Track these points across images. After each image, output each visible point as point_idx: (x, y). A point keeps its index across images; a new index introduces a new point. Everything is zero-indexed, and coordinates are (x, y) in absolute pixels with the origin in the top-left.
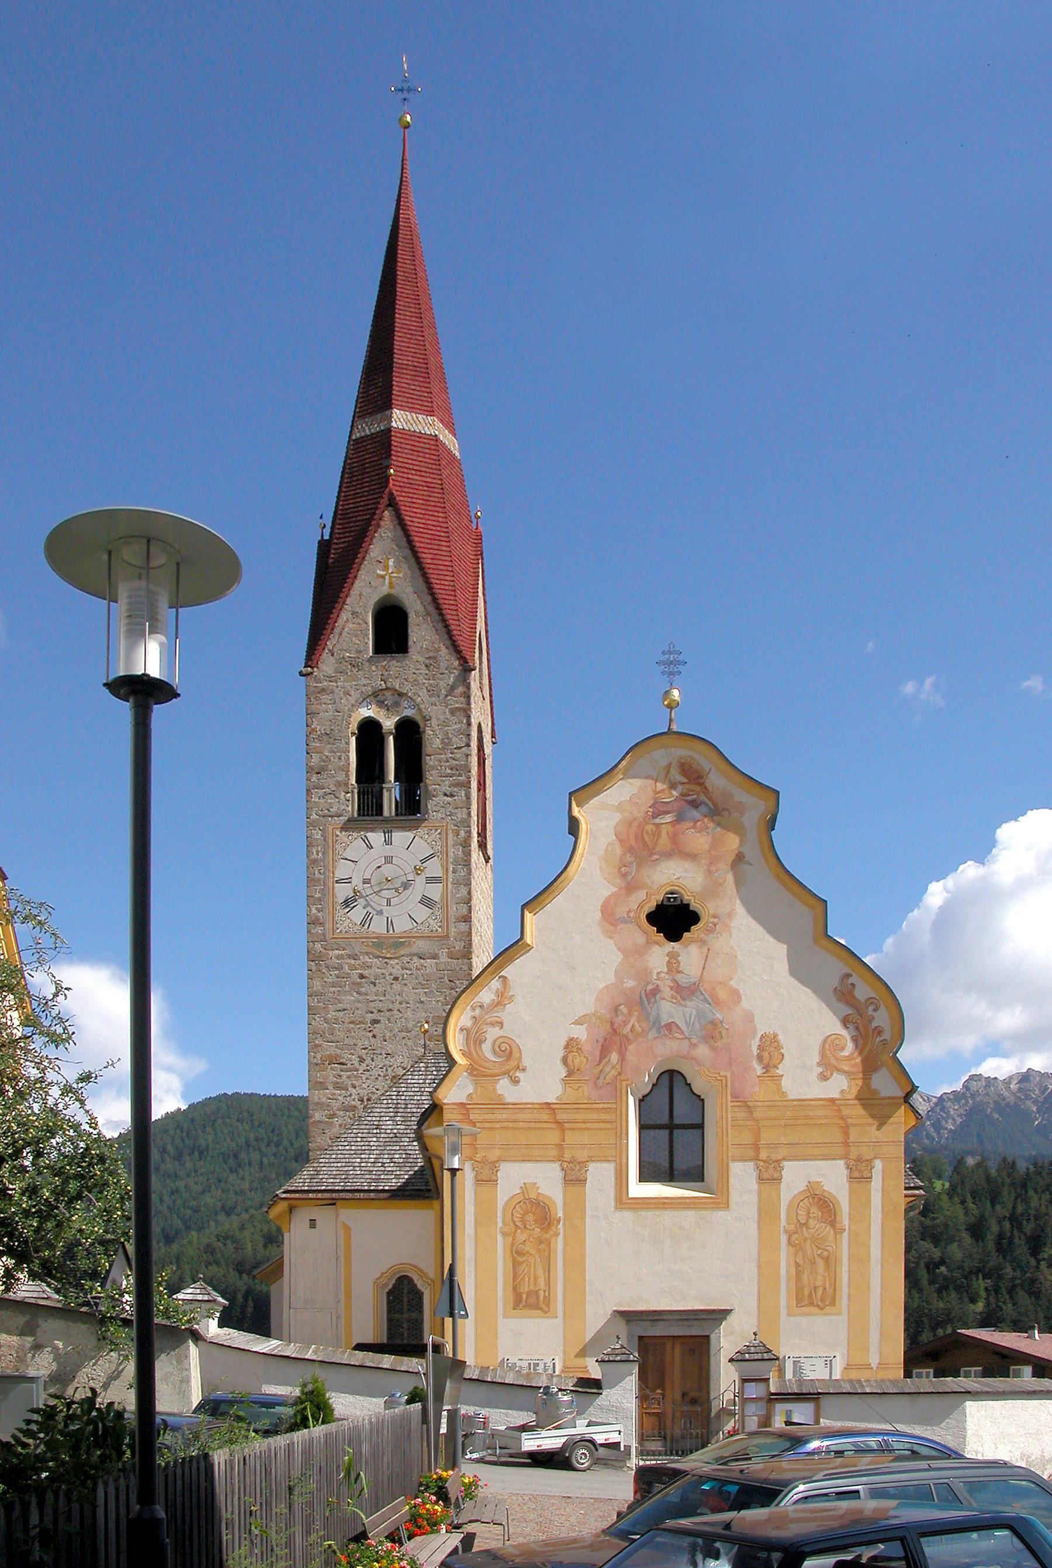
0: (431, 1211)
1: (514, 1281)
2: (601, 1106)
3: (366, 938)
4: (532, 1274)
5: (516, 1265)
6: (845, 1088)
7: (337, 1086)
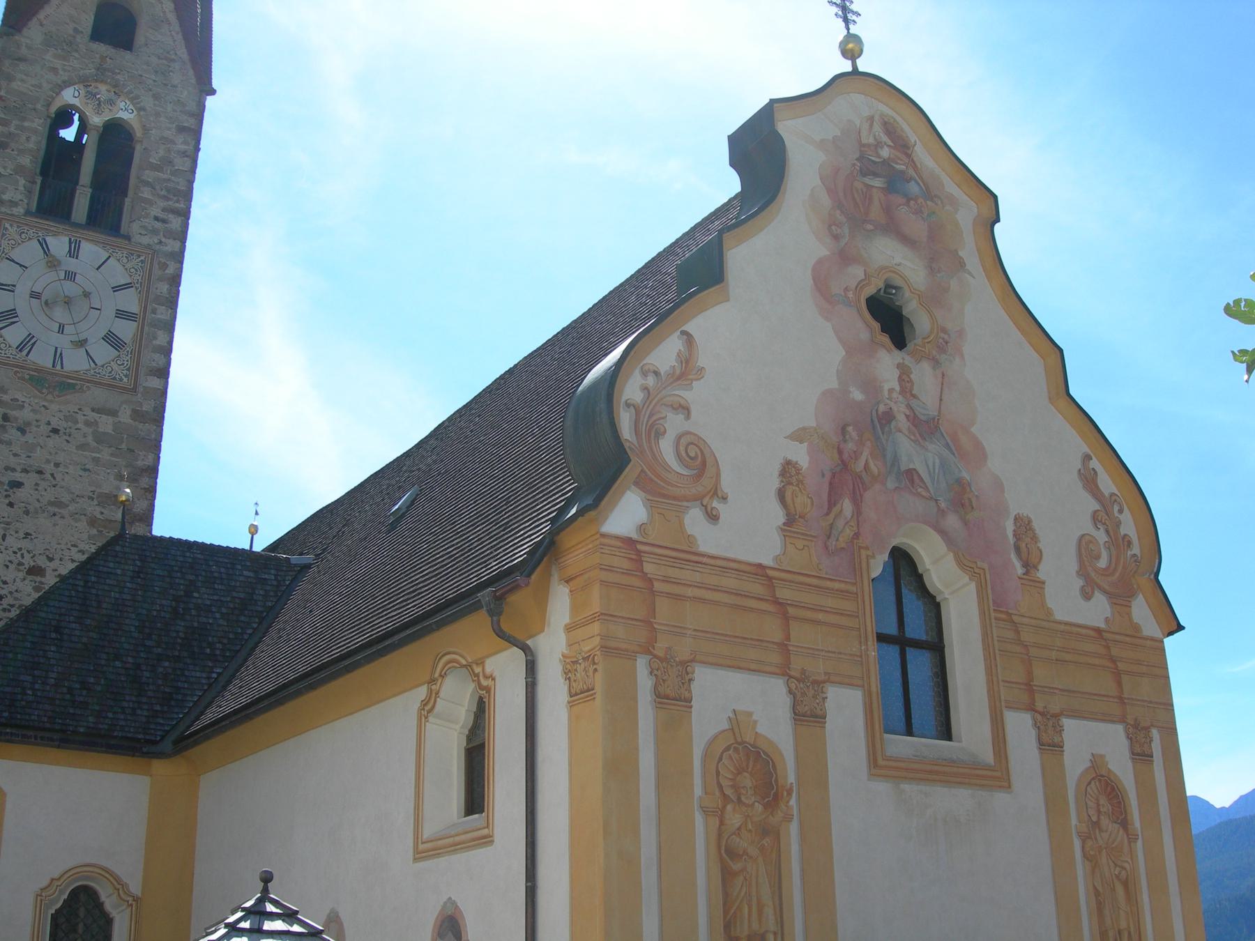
0: (146, 780)
1: (726, 912)
2: (837, 585)
4: (754, 900)
5: (727, 876)
6: (1109, 615)
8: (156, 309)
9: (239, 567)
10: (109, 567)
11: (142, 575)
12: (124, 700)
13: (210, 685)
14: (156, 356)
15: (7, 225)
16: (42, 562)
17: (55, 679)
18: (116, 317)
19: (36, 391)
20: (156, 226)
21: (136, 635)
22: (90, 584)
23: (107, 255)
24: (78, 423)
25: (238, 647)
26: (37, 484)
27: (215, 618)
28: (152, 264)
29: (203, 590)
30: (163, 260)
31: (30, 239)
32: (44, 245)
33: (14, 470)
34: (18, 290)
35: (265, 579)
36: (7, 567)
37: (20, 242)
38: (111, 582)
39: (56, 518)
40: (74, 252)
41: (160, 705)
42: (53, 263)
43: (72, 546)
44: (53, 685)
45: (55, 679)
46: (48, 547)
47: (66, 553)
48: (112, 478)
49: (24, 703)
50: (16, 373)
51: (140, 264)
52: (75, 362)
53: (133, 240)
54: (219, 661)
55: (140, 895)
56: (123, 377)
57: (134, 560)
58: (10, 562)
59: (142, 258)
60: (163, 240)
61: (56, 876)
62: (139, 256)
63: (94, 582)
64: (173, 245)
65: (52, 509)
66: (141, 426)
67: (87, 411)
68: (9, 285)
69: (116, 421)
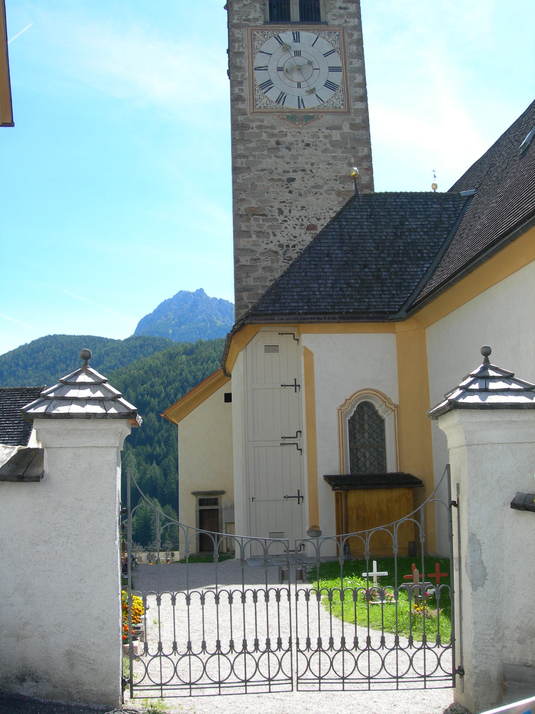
3: (282, 112)
7: (259, 233)
8: (352, 62)
9: (430, 203)
10: (352, 215)
11: (372, 217)
12: (374, 291)
13: (423, 275)
14: (358, 89)
15: (255, 33)
16: (314, 222)
17: (331, 284)
18: (329, 71)
19: (292, 124)
20: (341, 13)
21: (374, 252)
22: (343, 226)
23: (316, 36)
24: (319, 137)
25: (437, 251)
26: (303, 178)
27: (421, 235)
28: (344, 36)
29: (410, 220)
30: (349, 32)
31: (270, 37)
32: (278, 38)
33: (288, 172)
34: (269, 68)
35: (447, 207)
36: (295, 228)
37: (265, 40)
38: (355, 223)
39: (318, 195)
40: (297, 39)
41: (395, 290)
42: (286, 48)
43: (330, 209)
44: (330, 287)
45: (331, 284)
46: (316, 213)
47: (327, 214)
48: (345, 166)
49: (315, 300)
50: (278, 116)
51: (336, 37)
52: (311, 103)
53: (329, 24)
54: (427, 260)
55: (398, 404)
56: (341, 106)
57: (367, 209)
58: (296, 224)
59: (337, 33)
60: (347, 20)
61: (348, 398)
62: (335, 33)
63: (345, 225)
64: (353, 22)
65: (315, 190)
66: (356, 132)
67: (324, 130)
68: (264, 67)
69: (341, 132)
